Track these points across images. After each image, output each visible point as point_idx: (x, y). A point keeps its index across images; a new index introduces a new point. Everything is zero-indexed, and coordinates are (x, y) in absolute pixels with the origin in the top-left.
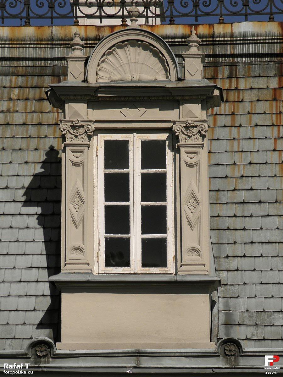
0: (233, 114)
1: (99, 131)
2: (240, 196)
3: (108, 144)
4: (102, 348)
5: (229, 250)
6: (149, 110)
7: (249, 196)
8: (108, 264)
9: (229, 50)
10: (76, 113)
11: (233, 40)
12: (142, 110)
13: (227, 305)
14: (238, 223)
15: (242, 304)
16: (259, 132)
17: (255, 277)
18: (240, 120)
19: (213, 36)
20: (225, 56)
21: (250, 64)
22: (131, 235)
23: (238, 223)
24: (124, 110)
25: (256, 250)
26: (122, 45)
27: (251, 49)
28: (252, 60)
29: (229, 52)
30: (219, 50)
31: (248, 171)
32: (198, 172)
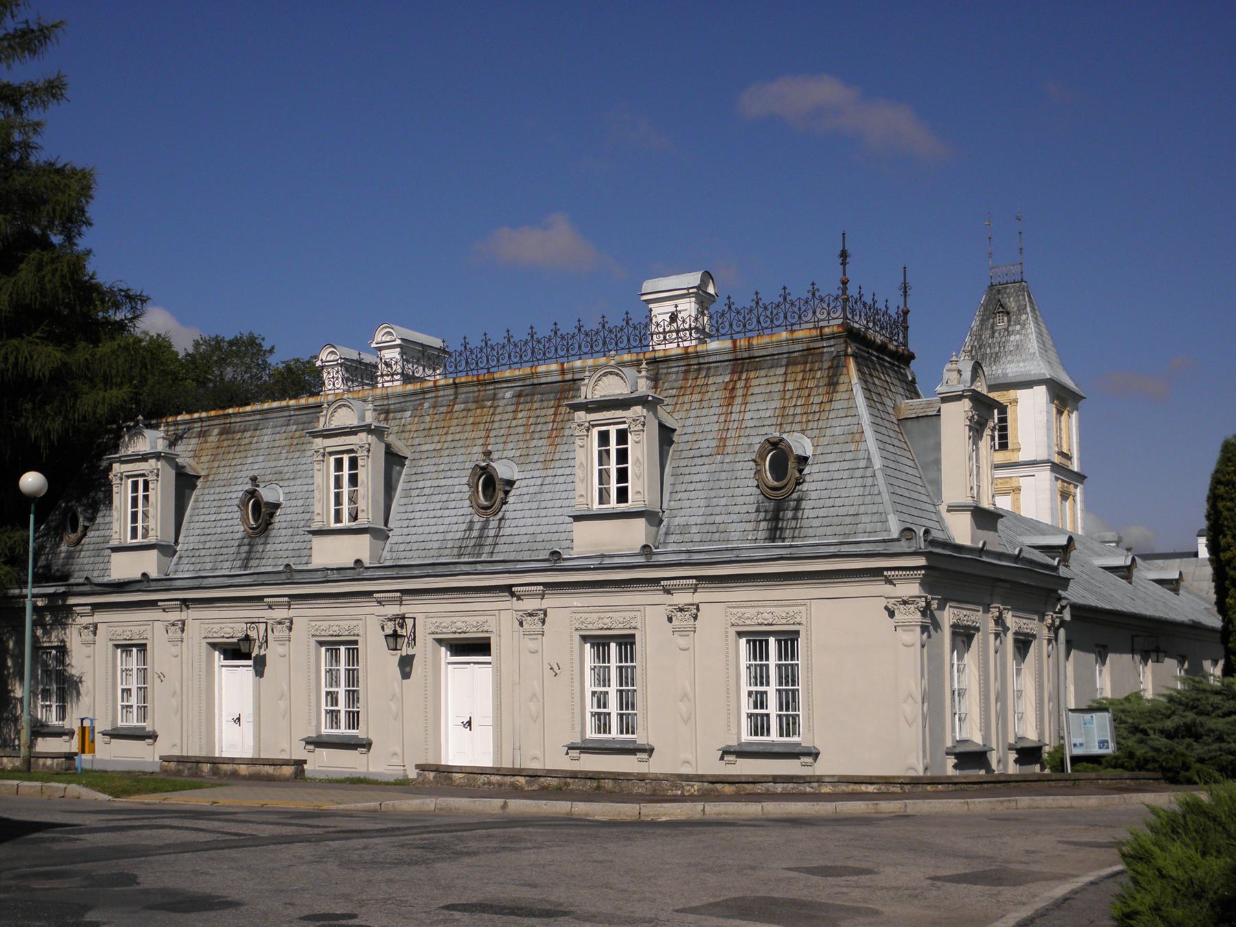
0: (701, 400)
1: (594, 426)
2: (692, 453)
3: (336, 459)
4: (629, 550)
5: (678, 488)
6: (617, 412)
7: (696, 453)
8: (618, 502)
9: (706, 360)
10: (579, 418)
11: (708, 354)
12: (613, 411)
13: (669, 522)
14: (687, 470)
15: (677, 521)
16: (712, 411)
17: (687, 503)
18: (705, 404)
19: (697, 352)
20: (705, 363)
21: (718, 367)
22: (344, 507)
23: (687, 470)
24: (604, 413)
25: (691, 487)
26: (605, 375)
27: (718, 358)
28: (719, 364)
29: (706, 361)
30: (701, 360)
31: (701, 437)
32: (368, 469)
